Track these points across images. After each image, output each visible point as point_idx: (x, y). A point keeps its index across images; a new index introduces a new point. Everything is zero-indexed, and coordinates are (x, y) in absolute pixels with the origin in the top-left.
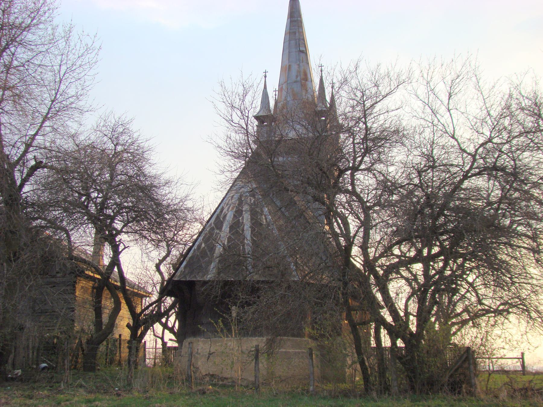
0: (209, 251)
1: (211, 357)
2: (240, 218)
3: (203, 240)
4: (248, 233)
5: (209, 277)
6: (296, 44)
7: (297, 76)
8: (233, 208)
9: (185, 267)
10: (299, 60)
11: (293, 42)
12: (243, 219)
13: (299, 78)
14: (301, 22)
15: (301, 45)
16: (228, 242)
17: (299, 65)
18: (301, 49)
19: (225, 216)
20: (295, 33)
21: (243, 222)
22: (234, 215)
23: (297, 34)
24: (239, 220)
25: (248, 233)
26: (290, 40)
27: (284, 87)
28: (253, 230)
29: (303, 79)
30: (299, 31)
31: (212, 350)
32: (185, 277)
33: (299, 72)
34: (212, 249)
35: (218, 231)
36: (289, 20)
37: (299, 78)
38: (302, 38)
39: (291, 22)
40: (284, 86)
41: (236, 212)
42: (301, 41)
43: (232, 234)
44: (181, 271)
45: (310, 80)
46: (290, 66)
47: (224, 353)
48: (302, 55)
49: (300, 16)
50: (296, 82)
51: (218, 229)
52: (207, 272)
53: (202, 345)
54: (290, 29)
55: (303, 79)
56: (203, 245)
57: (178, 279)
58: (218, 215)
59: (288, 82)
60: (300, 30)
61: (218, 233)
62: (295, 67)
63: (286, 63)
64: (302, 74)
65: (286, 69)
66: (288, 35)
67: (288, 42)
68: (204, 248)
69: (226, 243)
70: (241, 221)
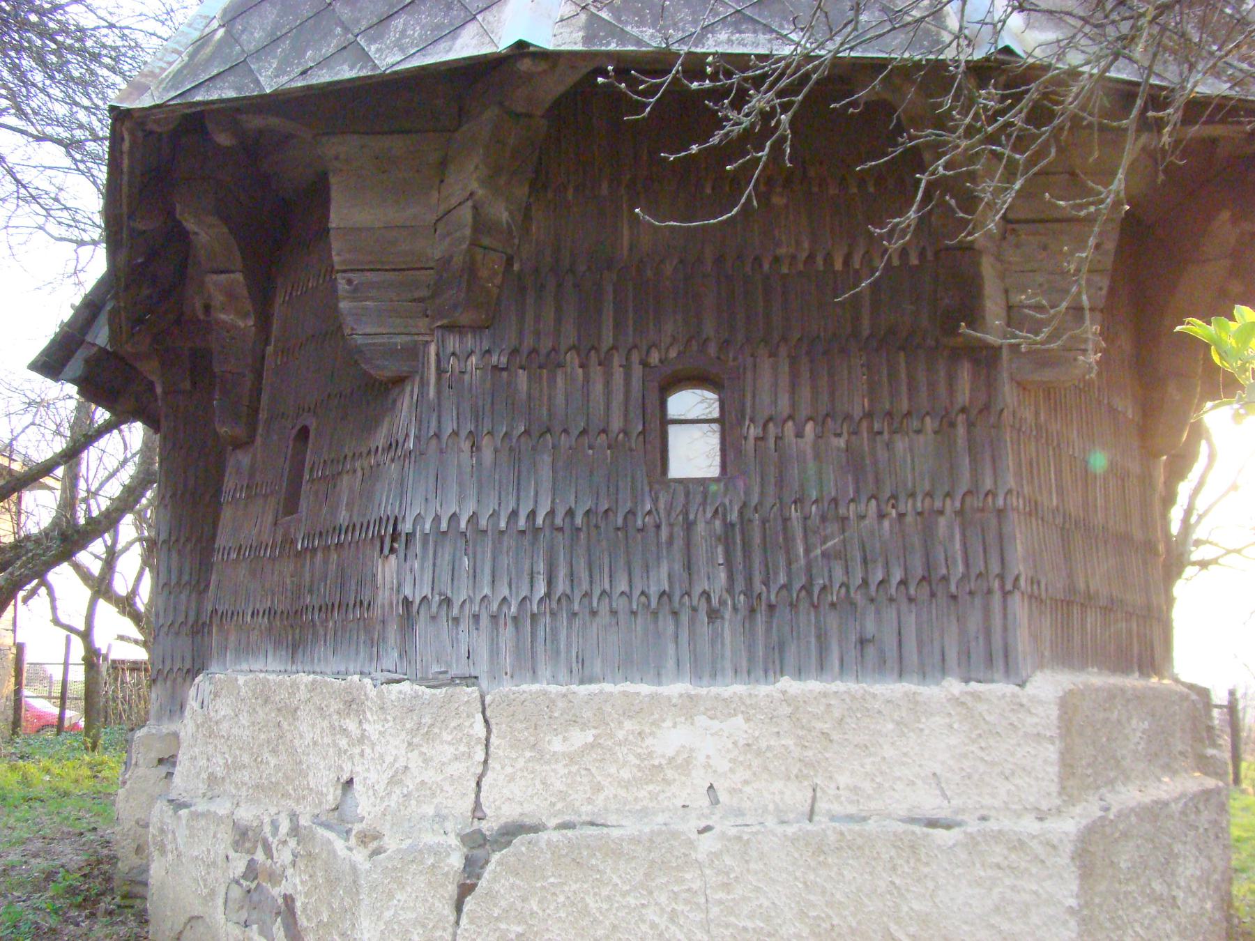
31: (507, 799)
32: (239, 67)
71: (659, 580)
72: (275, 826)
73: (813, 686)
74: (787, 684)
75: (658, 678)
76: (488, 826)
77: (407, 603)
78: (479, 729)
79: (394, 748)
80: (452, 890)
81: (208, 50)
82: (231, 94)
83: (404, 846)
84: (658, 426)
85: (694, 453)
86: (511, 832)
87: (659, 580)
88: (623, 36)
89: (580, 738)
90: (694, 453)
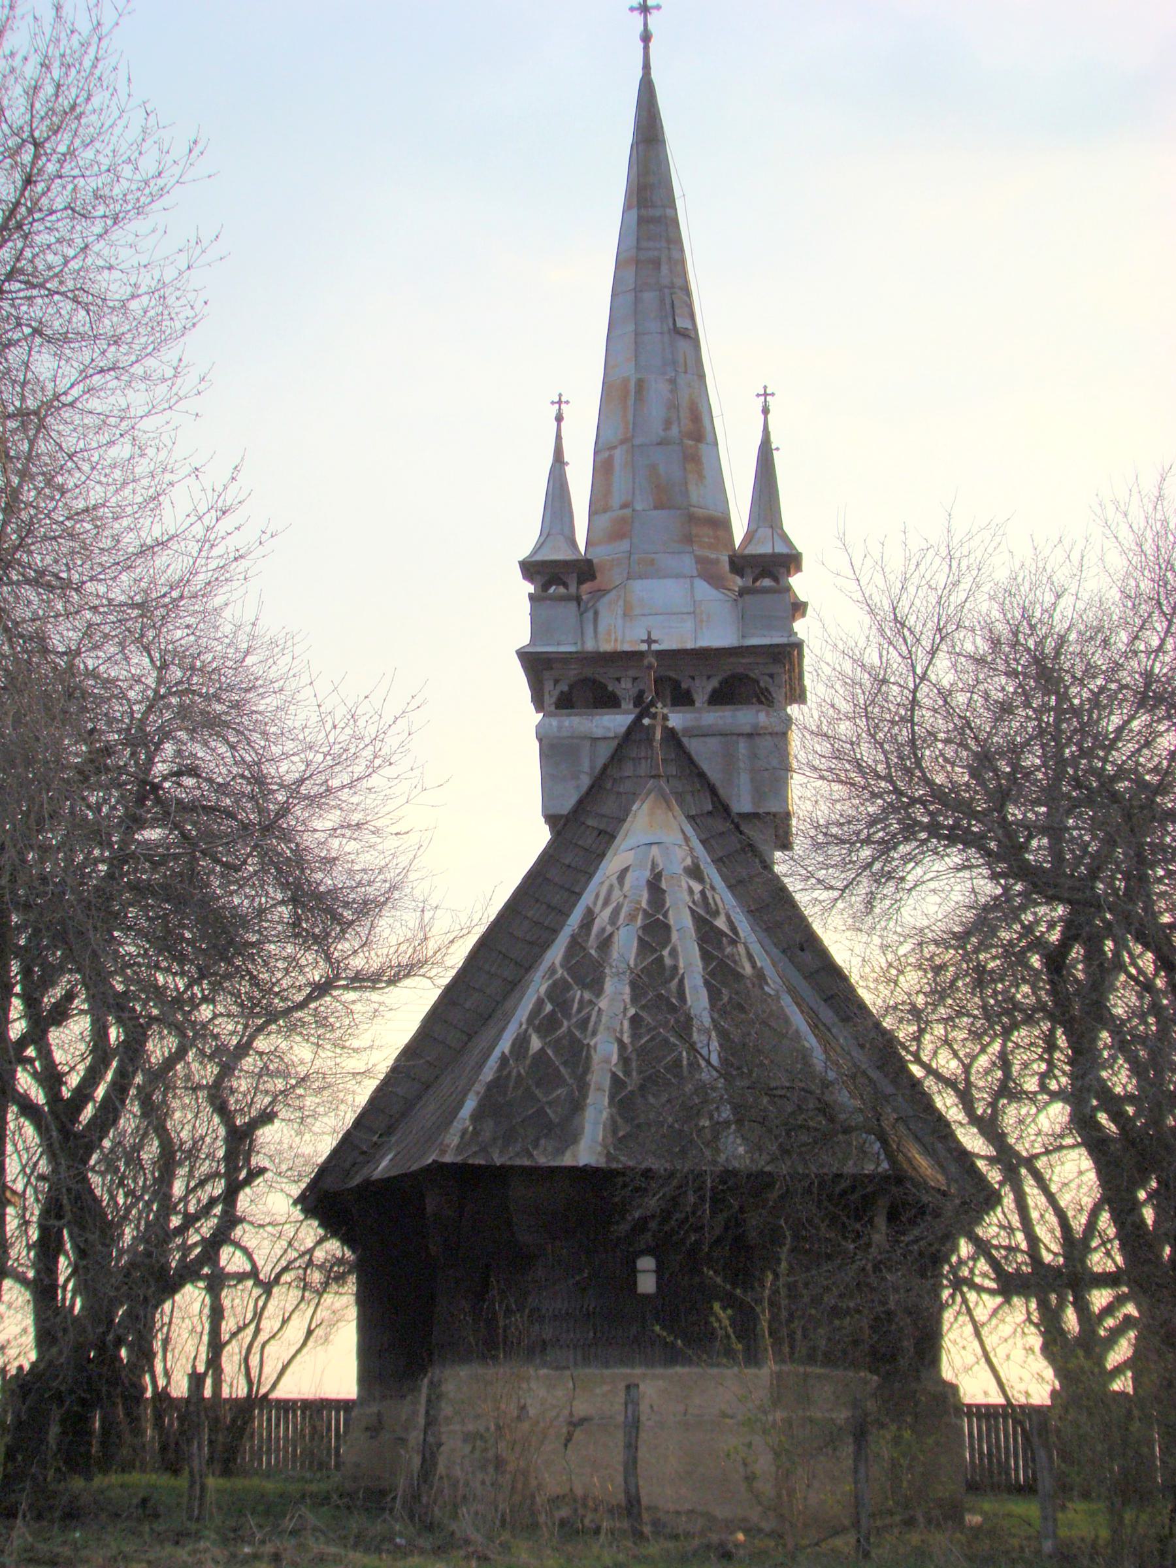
0: (565, 1063)
1: (578, 1435)
2: (665, 953)
3: (530, 1021)
4: (698, 1001)
6: (662, 301)
7: (668, 424)
8: (632, 917)
9: (477, 1117)
10: (674, 363)
11: (649, 296)
12: (674, 953)
13: (675, 431)
15: (677, 311)
16: (635, 1036)
17: (673, 381)
18: (680, 323)
19: (606, 943)
20: (656, 264)
22: (640, 939)
23: (665, 269)
24: (661, 958)
25: (698, 1001)
26: (637, 290)
28: (714, 995)
30: (670, 258)
31: (581, 1408)
32: (484, 1149)
34: (577, 1054)
35: (587, 996)
36: (634, 213)
37: (675, 431)
38: (678, 282)
39: (641, 221)
40: (617, 453)
41: (645, 928)
43: (643, 1007)
44: (464, 1132)
45: (709, 439)
46: (640, 385)
47: (547, 1412)
48: (683, 345)
51: (584, 986)
53: (465, 1390)
54: (639, 249)
56: (536, 1043)
57: (459, 1159)
59: (637, 442)
62: (658, 389)
64: (684, 414)
65: (621, 395)
67: (630, 298)
69: (626, 1039)
70: (668, 961)
71: (634, 1330)
72: (488, 1429)
73: (686, 1370)
74: (679, 1369)
75: (633, 1367)
76: (575, 1419)
77: (544, 1342)
78: (571, 1385)
79: (542, 1392)
80: (562, 1440)
81: (467, 1136)
82: (483, 1162)
83: (768, 1169)
84: (633, 1272)
85: (647, 1284)
86: (583, 1420)
87: (634, 1330)
88: (618, 1161)
89: (606, 1388)
90: (647, 1284)
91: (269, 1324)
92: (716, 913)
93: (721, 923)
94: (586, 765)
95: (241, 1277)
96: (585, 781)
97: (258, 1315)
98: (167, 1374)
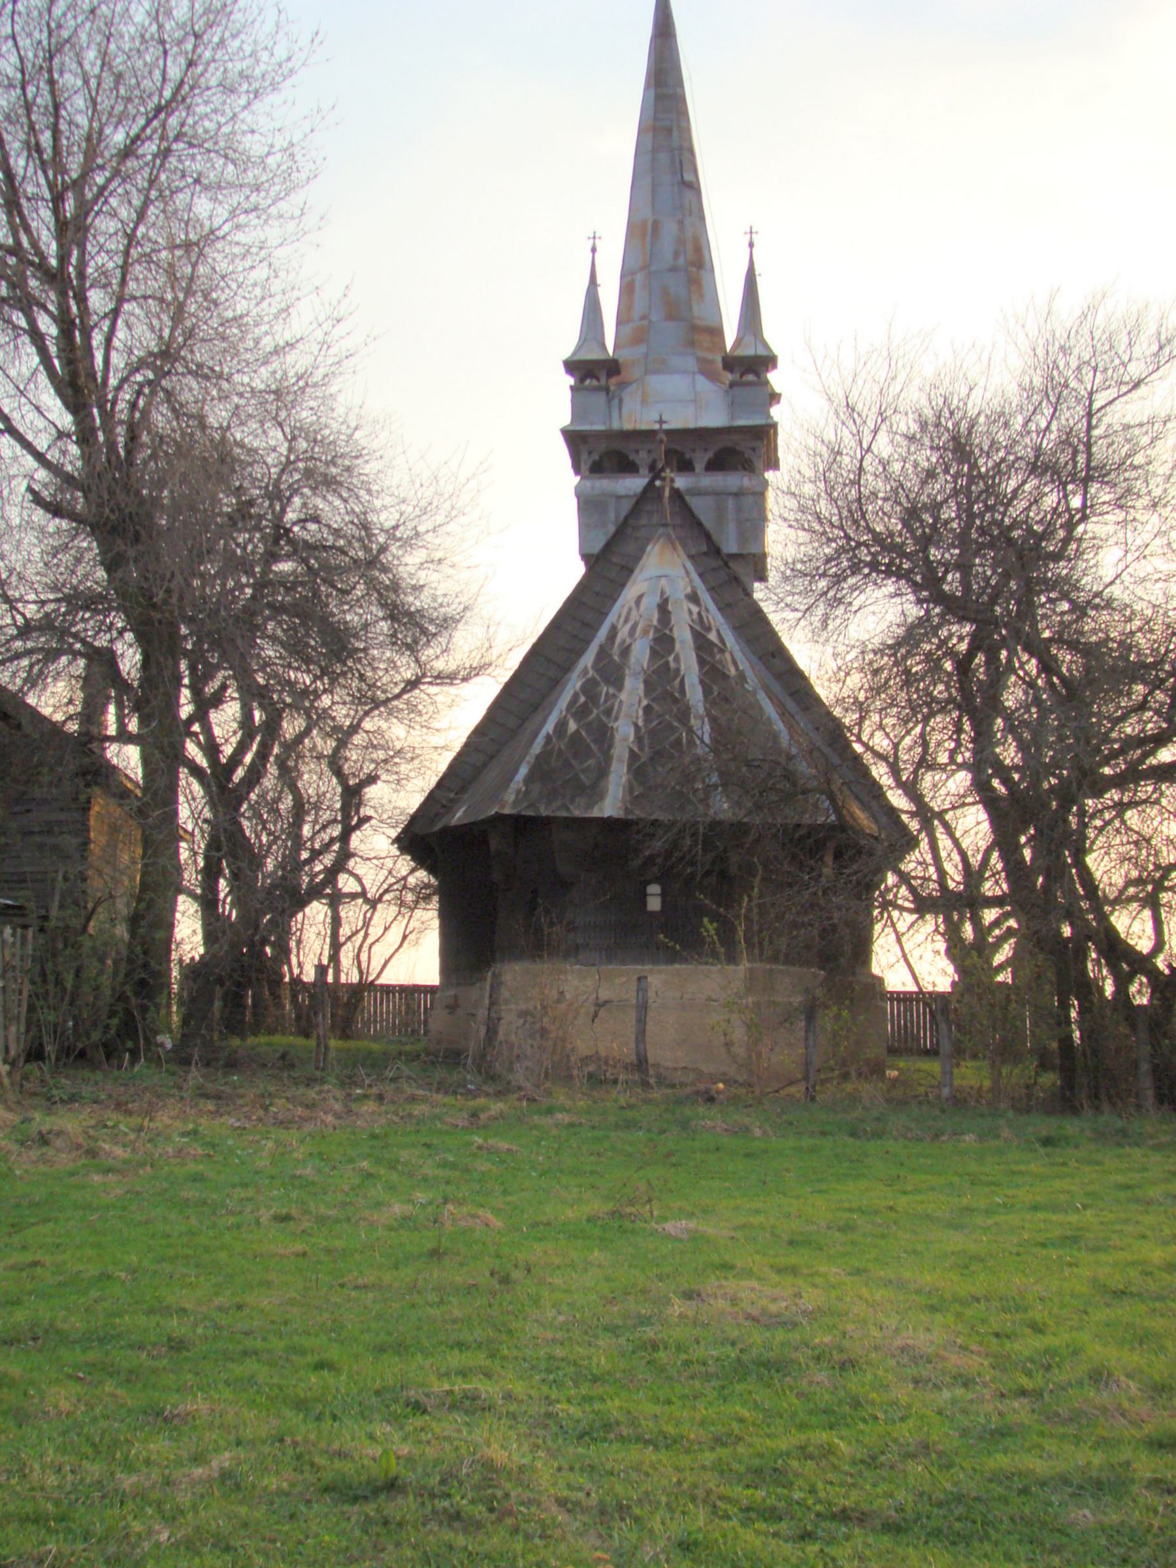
0: (595, 741)
2: (671, 659)
4: (695, 694)
5: (610, 806)
7: (676, 255)
8: (645, 632)
9: (528, 780)
11: (664, 157)
13: (681, 261)
14: (682, 99)
17: (681, 223)
19: (626, 651)
20: (669, 131)
21: (678, 670)
23: (675, 134)
24: (667, 663)
25: (695, 694)
26: (655, 151)
27: (639, 278)
28: (707, 691)
29: (693, 264)
31: (604, 994)
33: (681, 241)
34: (604, 736)
35: (611, 691)
36: (652, 92)
41: (655, 640)
42: (687, 154)
44: (518, 792)
45: (708, 265)
46: (656, 226)
49: (680, 83)
50: (673, 269)
51: (608, 682)
52: (595, 792)
53: (519, 981)
54: (656, 119)
55: (693, 264)
56: (572, 726)
57: (514, 812)
58: (601, 647)
59: (653, 268)
60: (683, 124)
61: (614, 696)
62: (670, 229)
63: (647, 214)
64: (689, 247)
65: (642, 233)
66: (650, 135)
68: (577, 732)
69: (640, 723)
91: (375, 931)
92: (709, 629)
93: (712, 636)
94: (612, 515)
95: (353, 896)
96: (612, 529)
97: (367, 924)
98: (300, 965)
